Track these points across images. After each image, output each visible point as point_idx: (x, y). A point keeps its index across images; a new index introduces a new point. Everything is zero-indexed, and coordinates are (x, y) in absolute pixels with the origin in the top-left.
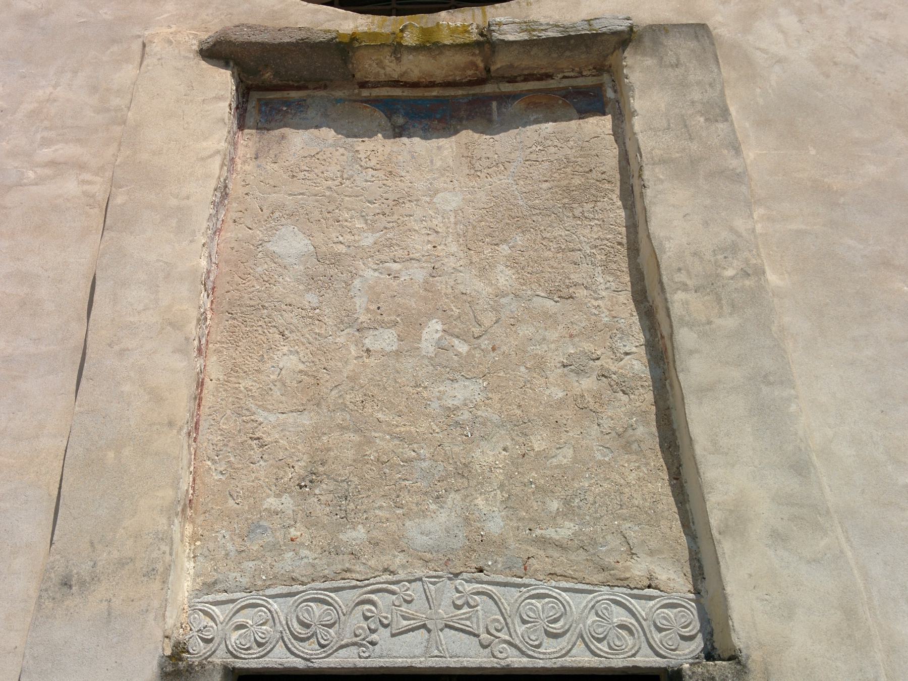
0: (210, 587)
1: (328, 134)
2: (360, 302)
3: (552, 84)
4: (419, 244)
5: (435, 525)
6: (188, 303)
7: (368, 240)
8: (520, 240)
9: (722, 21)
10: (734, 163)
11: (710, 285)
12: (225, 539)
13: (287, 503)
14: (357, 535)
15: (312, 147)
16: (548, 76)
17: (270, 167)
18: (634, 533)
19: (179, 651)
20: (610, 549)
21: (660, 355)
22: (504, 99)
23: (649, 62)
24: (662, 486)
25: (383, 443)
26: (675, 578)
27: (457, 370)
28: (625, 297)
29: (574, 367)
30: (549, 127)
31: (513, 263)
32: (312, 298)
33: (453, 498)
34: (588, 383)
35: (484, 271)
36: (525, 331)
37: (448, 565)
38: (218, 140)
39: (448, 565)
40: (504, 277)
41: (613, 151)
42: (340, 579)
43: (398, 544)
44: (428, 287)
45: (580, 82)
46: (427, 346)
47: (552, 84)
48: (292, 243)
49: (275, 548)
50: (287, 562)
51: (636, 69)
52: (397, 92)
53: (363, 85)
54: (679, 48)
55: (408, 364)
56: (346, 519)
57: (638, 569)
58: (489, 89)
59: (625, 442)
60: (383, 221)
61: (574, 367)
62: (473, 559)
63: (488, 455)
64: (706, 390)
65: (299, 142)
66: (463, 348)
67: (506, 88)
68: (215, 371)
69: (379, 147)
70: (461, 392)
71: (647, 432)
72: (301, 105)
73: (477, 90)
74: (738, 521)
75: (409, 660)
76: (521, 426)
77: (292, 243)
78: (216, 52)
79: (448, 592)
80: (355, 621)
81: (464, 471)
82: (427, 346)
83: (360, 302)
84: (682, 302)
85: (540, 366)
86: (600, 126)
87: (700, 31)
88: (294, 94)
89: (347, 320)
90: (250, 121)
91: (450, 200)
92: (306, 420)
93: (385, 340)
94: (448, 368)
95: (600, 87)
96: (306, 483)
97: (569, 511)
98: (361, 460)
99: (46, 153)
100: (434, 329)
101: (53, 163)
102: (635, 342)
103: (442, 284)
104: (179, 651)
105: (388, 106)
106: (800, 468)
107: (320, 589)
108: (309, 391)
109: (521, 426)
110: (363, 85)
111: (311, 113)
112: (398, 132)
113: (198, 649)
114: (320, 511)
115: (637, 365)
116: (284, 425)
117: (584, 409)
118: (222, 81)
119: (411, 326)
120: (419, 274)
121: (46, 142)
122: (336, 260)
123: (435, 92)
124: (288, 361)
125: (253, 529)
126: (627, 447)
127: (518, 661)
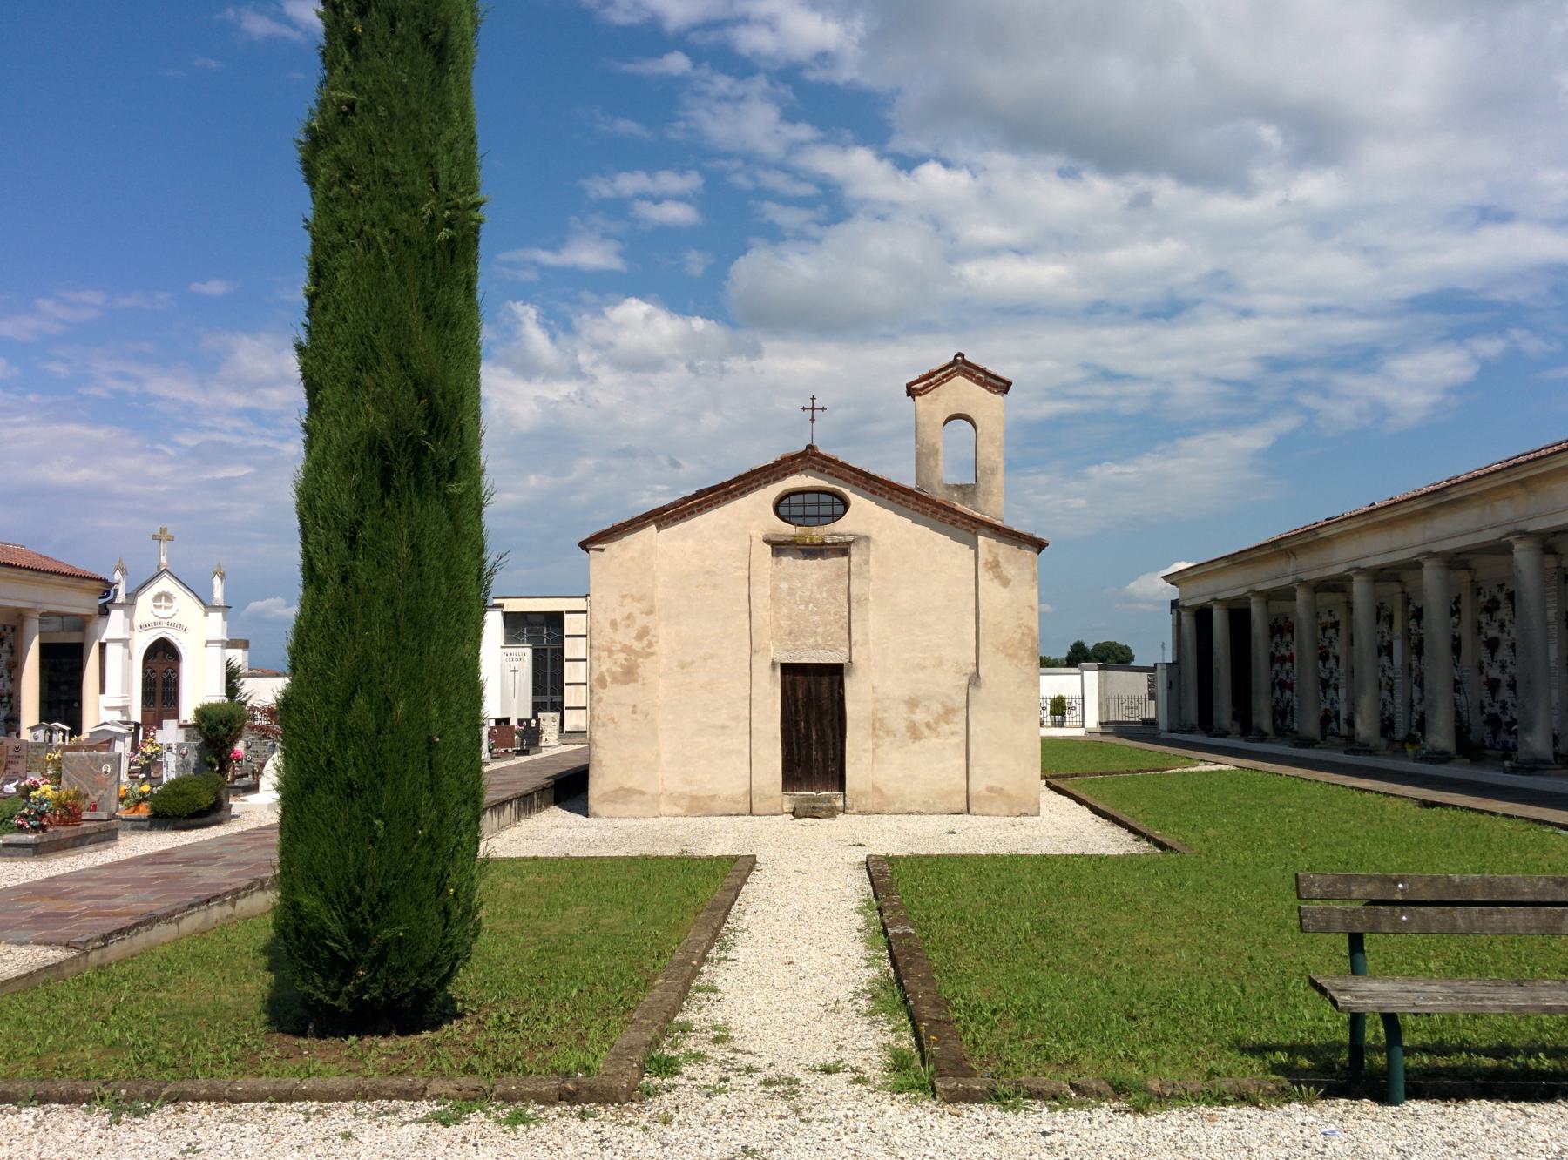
5: (811, 641)
6: (768, 601)
9: (874, 534)
19: (750, 863)
27: (816, 613)
38: (769, 564)
48: (784, 585)
51: (853, 550)
54: (863, 543)
62: (816, 646)
63: (820, 630)
65: (785, 560)
69: (801, 561)
70: (816, 618)
75: (1410, 987)
78: (767, 541)
87: (867, 538)
104: (750, 863)
105: (803, 551)
108: (789, 617)
116: (785, 623)
118: (769, 547)
119: (807, 604)
124: (785, 611)
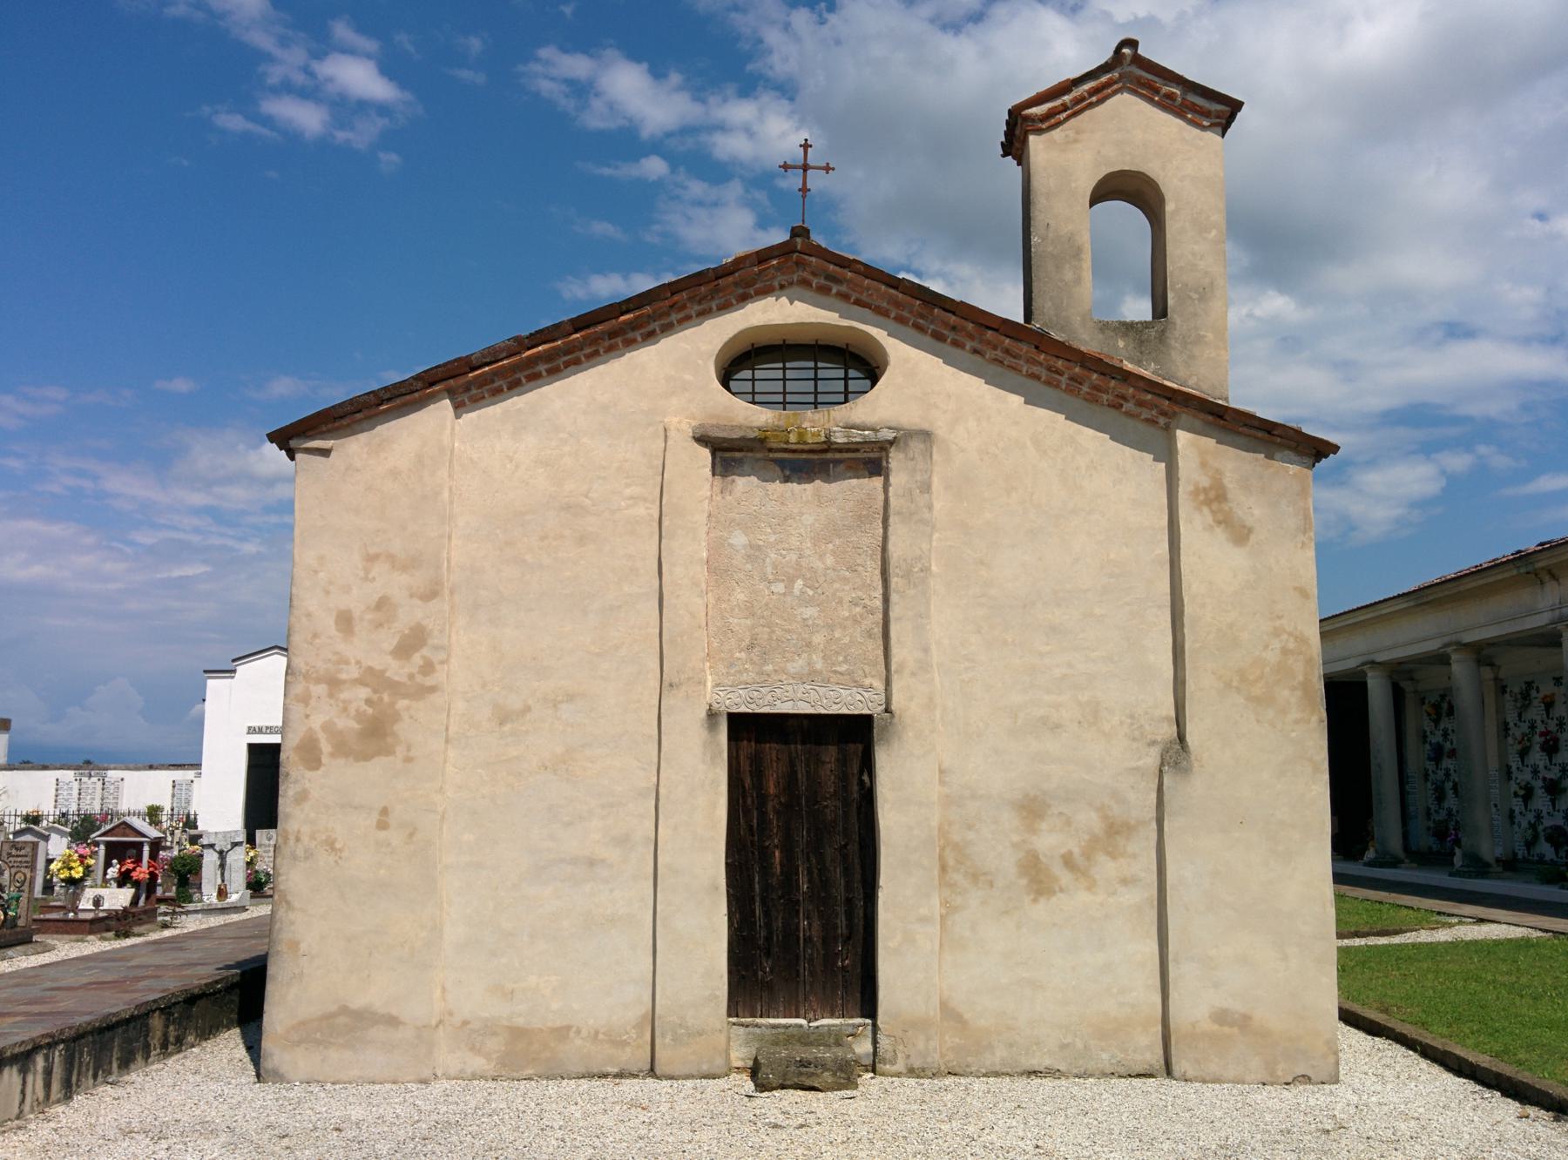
0: (718, 685)
1: (753, 479)
2: (769, 570)
3: (858, 455)
4: (794, 541)
6: (701, 573)
7: (772, 539)
8: (837, 542)
9: (940, 429)
10: (927, 515)
11: (907, 575)
12: (722, 668)
13: (743, 655)
14: (769, 668)
15: (744, 484)
16: (858, 450)
17: (729, 498)
18: (867, 669)
20: (858, 675)
21: (886, 600)
22: (837, 462)
23: (901, 456)
24: (880, 652)
25: (779, 632)
26: (879, 685)
27: (809, 602)
28: (878, 572)
29: (854, 603)
30: (854, 481)
31: (834, 553)
32: (749, 567)
33: (804, 655)
34: (858, 609)
35: (821, 557)
36: (836, 585)
37: (801, 678)
38: (706, 491)
39: (801, 678)
40: (830, 561)
41: (882, 497)
42: (763, 684)
43: (784, 671)
44: (798, 563)
45: (872, 455)
46: (796, 592)
47: (858, 455)
48: (739, 539)
49: (740, 672)
50: (744, 677)
51: (896, 460)
52: (786, 455)
53: (770, 450)
54: (916, 446)
55: (789, 599)
56: (765, 662)
57: (867, 682)
58: (829, 456)
59: (870, 635)
60: (779, 529)
61: (854, 603)
62: (810, 677)
63: (818, 639)
64: (899, 619)
66: (811, 593)
67: (838, 456)
68: (712, 601)
69: (777, 487)
70: (810, 612)
71: (878, 630)
72: (740, 462)
73: (824, 456)
74: (902, 666)
76: (831, 628)
77: (739, 539)
78: (702, 440)
79: (801, 688)
80: (769, 697)
81: (809, 645)
82: (796, 592)
83: (769, 570)
84: (894, 581)
85: (840, 602)
86: (878, 482)
87: (926, 436)
88: (738, 455)
89: (764, 578)
90: (718, 470)
91: (808, 519)
92: (749, 622)
93: (779, 588)
94: (806, 601)
95: (880, 459)
96: (751, 647)
97: (846, 661)
98: (770, 639)
99: (628, 492)
100: (800, 582)
101: (631, 498)
102: (878, 593)
103: (804, 562)
105: (781, 464)
106: (926, 650)
107: (23, 1092)
108: (749, 610)
109: (831, 628)
110: (770, 450)
111: (746, 467)
112: (787, 480)
113: (715, 706)
114: (756, 659)
115: (879, 603)
116: (740, 623)
117: (856, 621)
118: (706, 454)
119: (791, 581)
120: (793, 557)
121: (627, 486)
122: (759, 548)
123: (804, 456)
124: (740, 596)
125: (731, 665)
126: (870, 636)
127: (823, 712)
